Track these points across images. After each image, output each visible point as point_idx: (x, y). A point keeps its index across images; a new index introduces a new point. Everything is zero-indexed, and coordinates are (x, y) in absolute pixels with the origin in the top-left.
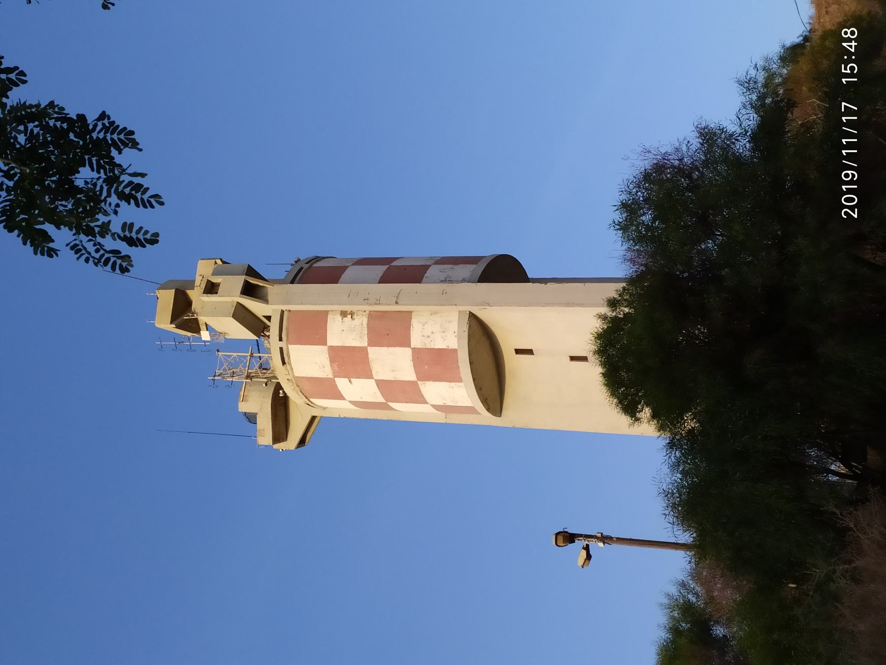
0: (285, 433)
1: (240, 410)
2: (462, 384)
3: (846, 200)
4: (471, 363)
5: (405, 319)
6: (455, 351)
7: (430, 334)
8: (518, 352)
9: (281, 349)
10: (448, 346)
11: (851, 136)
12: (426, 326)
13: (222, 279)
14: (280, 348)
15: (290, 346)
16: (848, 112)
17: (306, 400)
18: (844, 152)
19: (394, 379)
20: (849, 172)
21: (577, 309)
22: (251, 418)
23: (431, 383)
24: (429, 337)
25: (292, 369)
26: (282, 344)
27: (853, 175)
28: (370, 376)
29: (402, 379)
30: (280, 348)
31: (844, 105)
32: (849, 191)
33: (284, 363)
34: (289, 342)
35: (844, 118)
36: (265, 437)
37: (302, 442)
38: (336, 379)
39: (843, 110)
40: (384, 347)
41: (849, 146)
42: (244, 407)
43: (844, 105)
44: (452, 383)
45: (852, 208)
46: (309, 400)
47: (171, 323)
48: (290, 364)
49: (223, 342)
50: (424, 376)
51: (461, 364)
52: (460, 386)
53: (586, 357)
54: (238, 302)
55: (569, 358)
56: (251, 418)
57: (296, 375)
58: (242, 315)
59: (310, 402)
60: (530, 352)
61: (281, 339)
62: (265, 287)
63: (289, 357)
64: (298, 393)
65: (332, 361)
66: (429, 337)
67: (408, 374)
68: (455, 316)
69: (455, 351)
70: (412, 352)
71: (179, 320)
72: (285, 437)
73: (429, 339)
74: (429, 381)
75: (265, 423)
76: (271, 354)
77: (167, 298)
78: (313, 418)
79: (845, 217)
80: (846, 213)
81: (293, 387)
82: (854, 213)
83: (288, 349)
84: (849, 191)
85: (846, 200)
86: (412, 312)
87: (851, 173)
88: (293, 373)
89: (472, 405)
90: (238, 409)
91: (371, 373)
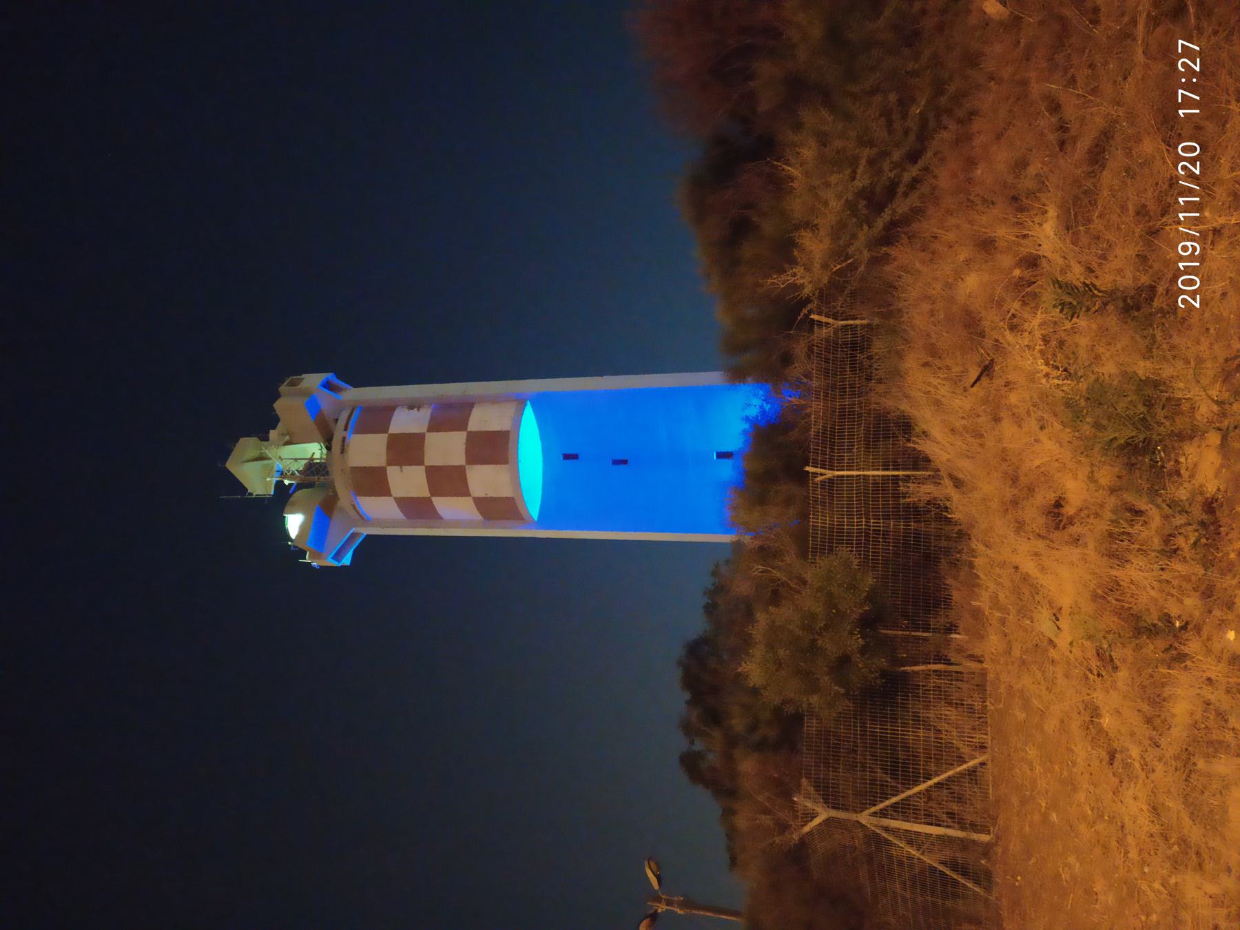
3: (1183, 283)
9: (344, 438)
10: (486, 494)
11: (1191, 192)
16: (1187, 103)
18: (1181, 215)
20: (1189, 244)
27: (1194, 249)
28: (469, 495)
31: (1182, 44)
32: (1188, 271)
35: (1181, 112)
38: (429, 495)
39: (1180, 101)
40: (441, 431)
41: (1189, 207)
43: (1182, 44)
45: (1193, 161)
49: (649, 919)
50: (436, 489)
53: (513, 499)
61: (346, 429)
69: (508, 432)
79: (1183, 70)
80: (1184, 301)
82: (1196, 65)
84: (1188, 271)
85: (1183, 283)
87: (1192, 246)
89: (512, 496)
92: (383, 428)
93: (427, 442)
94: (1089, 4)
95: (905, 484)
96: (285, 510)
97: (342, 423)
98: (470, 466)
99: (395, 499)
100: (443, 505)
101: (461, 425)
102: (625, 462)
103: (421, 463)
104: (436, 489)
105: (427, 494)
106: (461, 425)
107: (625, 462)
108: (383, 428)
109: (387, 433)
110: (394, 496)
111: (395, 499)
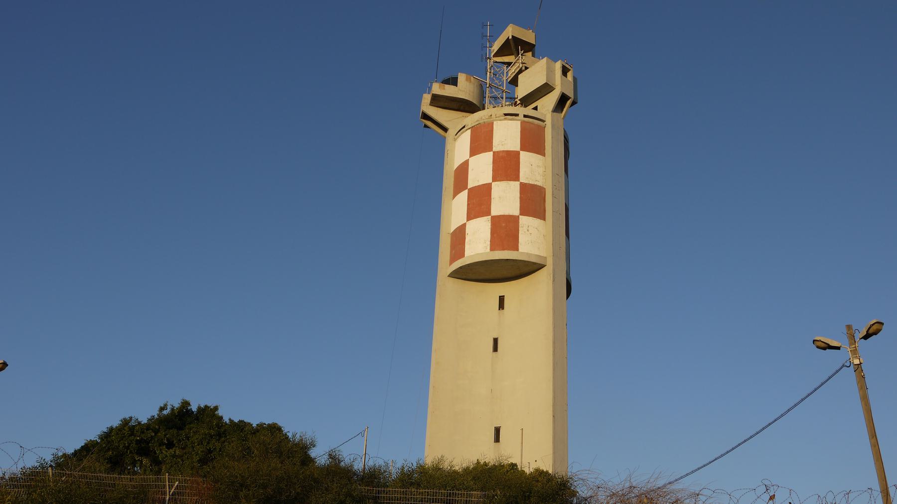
0: (436, 105)
1: (459, 74)
4: (507, 259)
5: (540, 214)
6: (516, 248)
7: (530, 231)
8: (502, 299)
9: (517, 115)
12: (536, 230)
13: (571, 80)
14: (518, 114)
15: (520, 122)
17: (470, 126)
19: (492, 197)
21: (551, 349)
22: (453, 81)
24: (528, 231)
25: (500, 120)
26: (521, 117)
30: (518, 114)
33: (506, 115)
34: (523, 123)
36: (437, 89)
37: (425, 116)
40: (520, 194)
42: (462, 78)
46: (469, 129)
47: (512, 36)
48: (505, 119)
50: (497, 222)
52: (486, 249)
54: (555, 89)
55: (496, 337)
56: (453, 81)
57: (495, 123)
58: (545, 90)
59: (467, 130)
60: (496, 341)
61: (525, 116)
62: (562, 112)
64: (477, 121)
65: (508, 153)
66: (528, 231)
67: (497, 209)
69: (517, 250)
70: (516, 216)
71: (512, 43)
73: (526, 230)
74: (491, 225)
75: (449, 91)
76: (488, 108)
77: (529, 36)
78: (445, 130)
81: (483, 118)
86: (545, 220)
88: (497, 120)
89: (465, 256)
90: (461, 72)
91: (498, 181)
93: (517, 182)
98: (490, 220)
99: (464, 225)
100: (464, 196)
102: (495, 349)
103: (495, 179)
105: (471, 184)
107: (495, 349)
109: (522, 149)
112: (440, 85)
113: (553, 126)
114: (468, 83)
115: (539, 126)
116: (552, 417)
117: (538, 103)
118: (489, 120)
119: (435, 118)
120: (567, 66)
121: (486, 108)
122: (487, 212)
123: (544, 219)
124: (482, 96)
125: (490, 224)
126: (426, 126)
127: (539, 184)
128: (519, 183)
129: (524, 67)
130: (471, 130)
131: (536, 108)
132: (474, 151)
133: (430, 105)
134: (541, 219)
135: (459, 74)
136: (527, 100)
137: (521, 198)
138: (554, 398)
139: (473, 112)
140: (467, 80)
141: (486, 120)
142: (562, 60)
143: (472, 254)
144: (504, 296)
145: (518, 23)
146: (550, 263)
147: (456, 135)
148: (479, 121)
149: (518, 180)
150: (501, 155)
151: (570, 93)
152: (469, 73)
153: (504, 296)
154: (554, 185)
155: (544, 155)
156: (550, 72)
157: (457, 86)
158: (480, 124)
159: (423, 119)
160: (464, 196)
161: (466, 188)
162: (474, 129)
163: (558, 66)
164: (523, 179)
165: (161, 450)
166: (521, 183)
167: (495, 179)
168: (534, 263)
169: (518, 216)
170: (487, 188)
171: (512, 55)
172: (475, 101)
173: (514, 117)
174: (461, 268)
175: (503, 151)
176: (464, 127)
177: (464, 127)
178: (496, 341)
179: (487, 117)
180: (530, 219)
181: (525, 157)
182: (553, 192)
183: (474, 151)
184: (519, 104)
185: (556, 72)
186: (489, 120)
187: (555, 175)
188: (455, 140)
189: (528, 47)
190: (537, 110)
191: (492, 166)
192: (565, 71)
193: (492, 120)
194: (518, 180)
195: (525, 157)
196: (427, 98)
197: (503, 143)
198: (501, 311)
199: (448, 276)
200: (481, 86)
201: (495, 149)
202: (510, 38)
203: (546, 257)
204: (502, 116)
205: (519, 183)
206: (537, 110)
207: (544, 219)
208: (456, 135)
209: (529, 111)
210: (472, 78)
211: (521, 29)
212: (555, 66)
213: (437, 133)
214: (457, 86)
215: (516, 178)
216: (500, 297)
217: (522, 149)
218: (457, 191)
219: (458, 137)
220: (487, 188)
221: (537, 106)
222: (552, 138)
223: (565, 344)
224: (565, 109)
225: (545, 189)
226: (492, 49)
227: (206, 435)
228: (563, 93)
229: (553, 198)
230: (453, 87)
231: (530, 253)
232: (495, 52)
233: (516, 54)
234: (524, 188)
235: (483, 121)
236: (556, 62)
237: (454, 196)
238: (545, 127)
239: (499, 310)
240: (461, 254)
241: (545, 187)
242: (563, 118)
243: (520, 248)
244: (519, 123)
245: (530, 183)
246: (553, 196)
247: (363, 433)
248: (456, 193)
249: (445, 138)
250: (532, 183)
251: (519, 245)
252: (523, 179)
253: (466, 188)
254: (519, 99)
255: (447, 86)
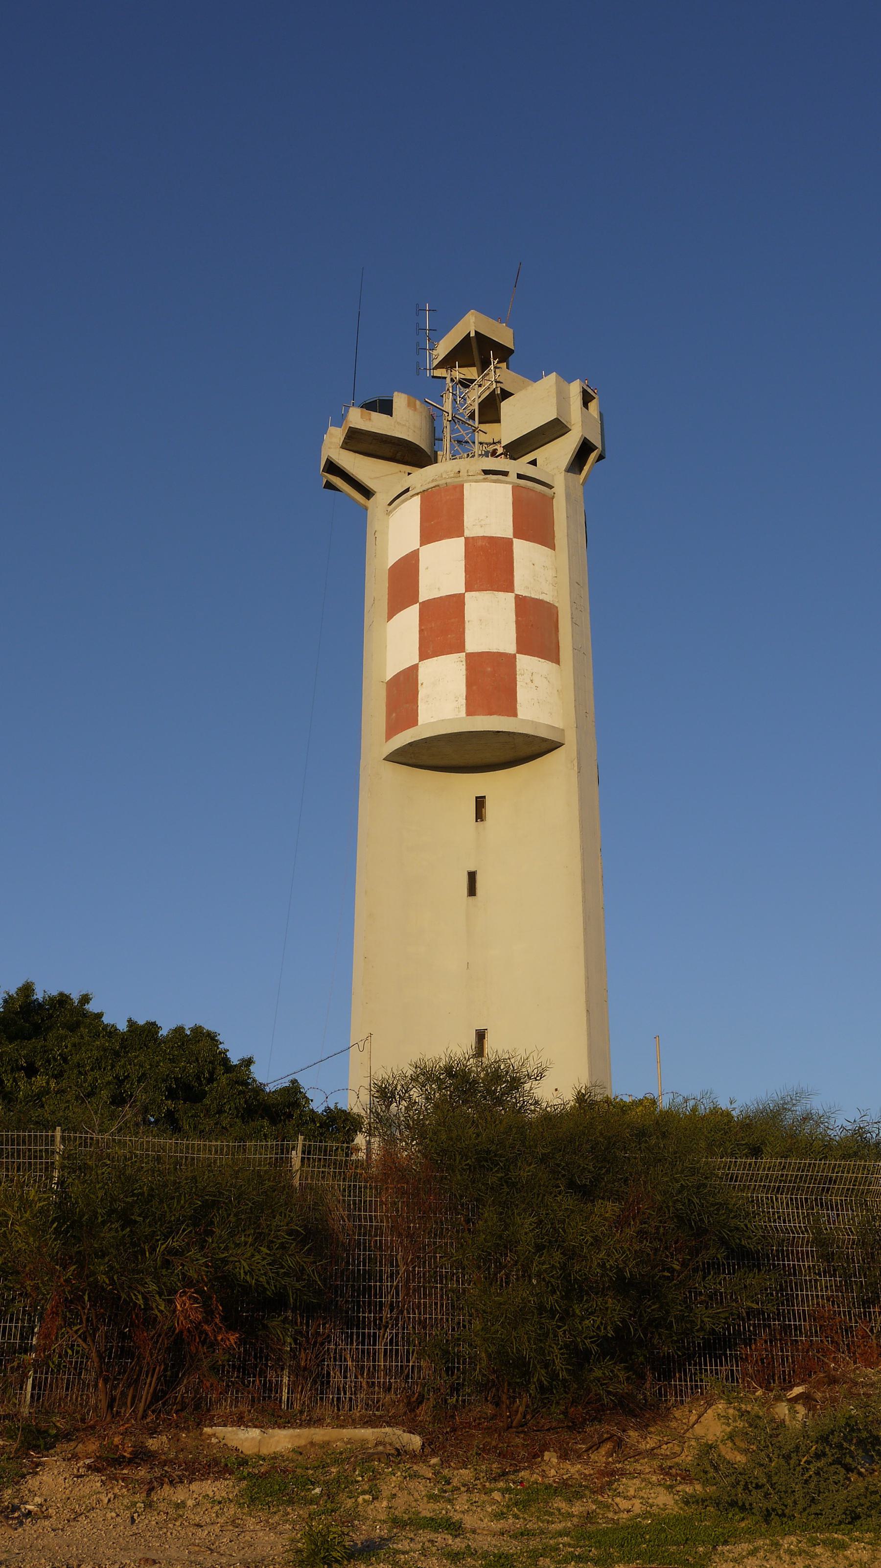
1: (396, 394)
2: (463, 713)
4: (498, 732)
5: (551, 653)
8: (480, 802)
9: (505, 474)
22: (386, 407)
23: (464, 672)
24: (532, 681)
25: (476, 481)
26: (513, 477)
29: (467, 631)
33: (486, 472)
34: (516, 489)
36: (357, 418)
37: (332, 468)
40: (517, 615)
42: (400, 401)
44: (465, 701)
46: (417, 494)
47: (476, 331)
48: (485, 480)
50: (430, 611)
51: (495, 718)
52: (459, 711)
55: (473, 870)
57: (466, 486)
59: (413, 496)
60: (472, 877)
61: (520, 476)
63: (495, 481)
64: (433, 481)
66: (532, 681)
68: (558, 723)
69: (515, 714)
72: (348, 447)
73: (529, 681)
74: (467, 670)
75: (377, 423)
77: (503, 335)
78: (367, 493)
83: (507, 483)
86: (559, 664)
89: (420, 723)
90: (398, 391)
92: (520, 531)
93: (501, 594)
94: (117, 1566)
95: (745, 1229)
96: (411, 398)
97: (530, 471)
98: (464, 659)
99: (414, 669)
100: (411, 616)
101: (526, 645)
102: (472, 891)
103: (469, 587)
104: (430, 611)
105: (424, 596)
106: (526, 645)
107: (472, 891)
108: (520, 531)
109: (516, 535)
110: (417, 662)
111: (414, 669)
112: (361, 411)
113: (568, 496)
114: (411, 412)
115: (544, 495)
116: (585, 1011)
117: (537, 454)
118: (456, 480)
119: (352, 471)
120: (589, 390)
121: (440, 458)
122: (458, 646)
123: (558, 662)
124: (435, 438)
125: (464, 667)
126: (329, 486)
127: (547, 598)
128: (513, 595)
129: (499, 389)
130: (421, 497)
131: (534, 463)
132: (428, 535)
133: (342, 447)
134: (552, 662)
135: (396, 394)
136: (515, 449)
137: (518, 623)
138: (587, 978)
139: (421, 466)
140: (409, 405)
141: (449, 481)
142: (583, 380)
143: (432, 720)
144: (484, 797)
145: (485, 310)
146: (571, 739)
147: (390, 504)
148: (436, 480)
149: (512, 591)
150: (480, 543)
151: (596, 440)
152: (414, 393)
153: (484, 797)
154: (573, 602)
155: (553, 547)
156: (562, 399)
157: (391, 416)
158: (438, 486)
159: (327, 472)
160: (411, 616)
161: (414, 599)
162: (429, 497)
163: (575, 389)
164: (520, 588)
165: (15, 1080)
166: (517, 596)
167: (469, 587)
168: (553, 741)
169: (514, 656)
170: (455, 604)
171: (472, 365)
172: (423, 445)
173: (500, 477)
174: (410, 744)
175: (484, 537)
176: (407, 490)
177: (407, 490)
178: (472, 877)
179: (452, 475)
180: (534, 660)
181: (523, 550)
182: (572, 614)
183: (428, 535)
184: (501, 454)
185: (572, 400)
186: (456, 480)
187: (574, 584)
188: (388, 513)
189: (504, 353)
190: (536, 465)
191: (463, 563)
192: (587, 399)
193: (461, 479)
194: (512, 591)
195: (523, 550)
196: (335, 436)
197: (483, 523)
198: (480, 823)
199: (384, 759)
200: (432, 419)
201: (467, 533)
202: (473, 334)
203: (563, 730)
204: (478, 474)
205: (513, 595)
206: (536, 465)
207: (558, 662)
208: (390, 504)
209: (521, 465)
210: (418, 403)
211: (491, 320)
212: (569, 390)
213: (354, 500)
214: (391, 416)
215: (507, 586)
216: (477, 798)
217: (516, 535)
218: (396, 606)
219: (395, 509)
220: (455, 604)
221: (536, 459)
222: (567, 517)
223: (600, 884)
224: (586, 468)
225: (557, 608)
226: (435, 352)
227: (105, 1050)
228: (585, 438)
229: (572, 627)
230: (384, 417)
231: (537, 720)
232: (440, 359)
233: (478, 362)
234: (524, 606)
235: (444, 482)
236: (570, 381)
237: (391, 614)
238: (553, 498)
239: (476, 821)
240: (412, 720)
241: (557, 605)
242: (583, 484)
243: (519, 712)
244: (510, 487)
245: (533, 597)
246: (572, 622)
247: (361, 1044)
248: (393, 612)
249: (366, 509)
250: (536, 597)
251: (518, 707)
252: (520, 588)
253: (416, 601)
254: (503, 444)
255: (375, 415)
